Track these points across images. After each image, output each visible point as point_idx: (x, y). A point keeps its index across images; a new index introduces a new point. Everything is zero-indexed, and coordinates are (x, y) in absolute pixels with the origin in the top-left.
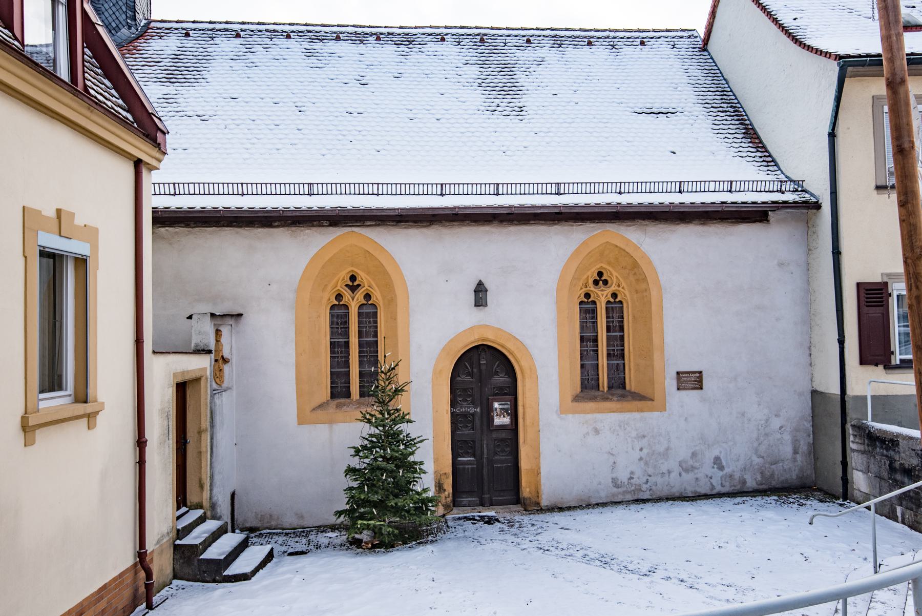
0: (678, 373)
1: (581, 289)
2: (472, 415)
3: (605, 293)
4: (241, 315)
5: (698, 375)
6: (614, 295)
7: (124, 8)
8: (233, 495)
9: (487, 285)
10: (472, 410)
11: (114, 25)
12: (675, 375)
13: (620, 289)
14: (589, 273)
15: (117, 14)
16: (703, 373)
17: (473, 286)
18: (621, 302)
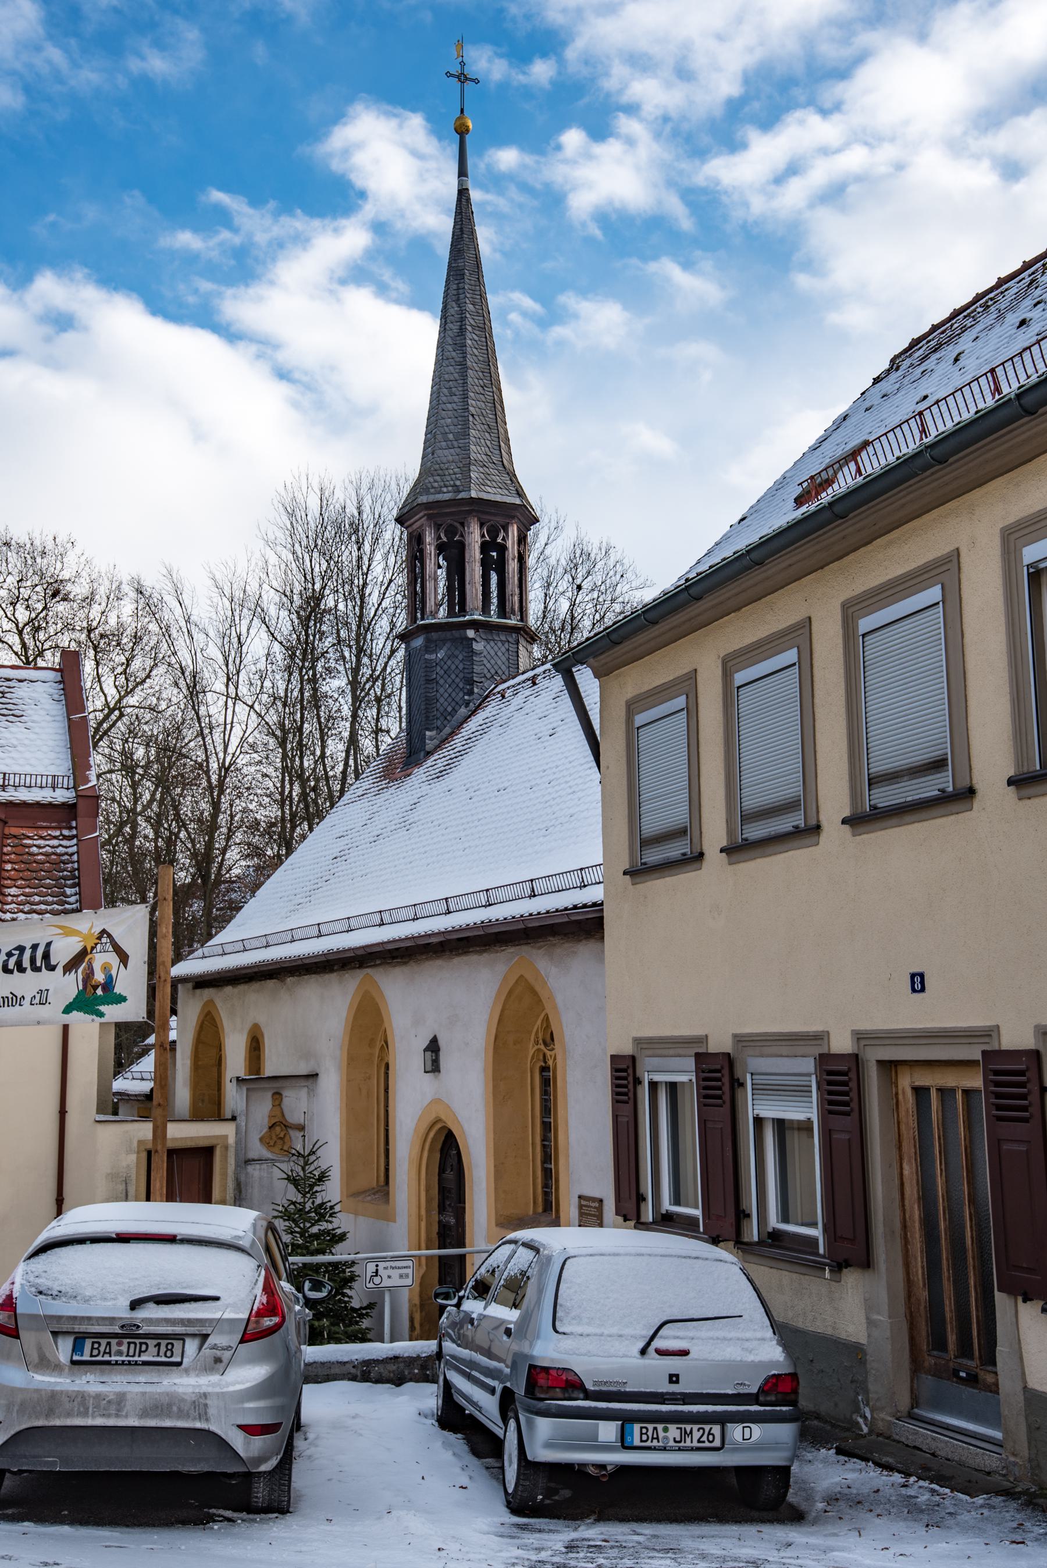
7: (461, 685)
9: (442, 1042)
11: (449, 709)
15: (454, 695)
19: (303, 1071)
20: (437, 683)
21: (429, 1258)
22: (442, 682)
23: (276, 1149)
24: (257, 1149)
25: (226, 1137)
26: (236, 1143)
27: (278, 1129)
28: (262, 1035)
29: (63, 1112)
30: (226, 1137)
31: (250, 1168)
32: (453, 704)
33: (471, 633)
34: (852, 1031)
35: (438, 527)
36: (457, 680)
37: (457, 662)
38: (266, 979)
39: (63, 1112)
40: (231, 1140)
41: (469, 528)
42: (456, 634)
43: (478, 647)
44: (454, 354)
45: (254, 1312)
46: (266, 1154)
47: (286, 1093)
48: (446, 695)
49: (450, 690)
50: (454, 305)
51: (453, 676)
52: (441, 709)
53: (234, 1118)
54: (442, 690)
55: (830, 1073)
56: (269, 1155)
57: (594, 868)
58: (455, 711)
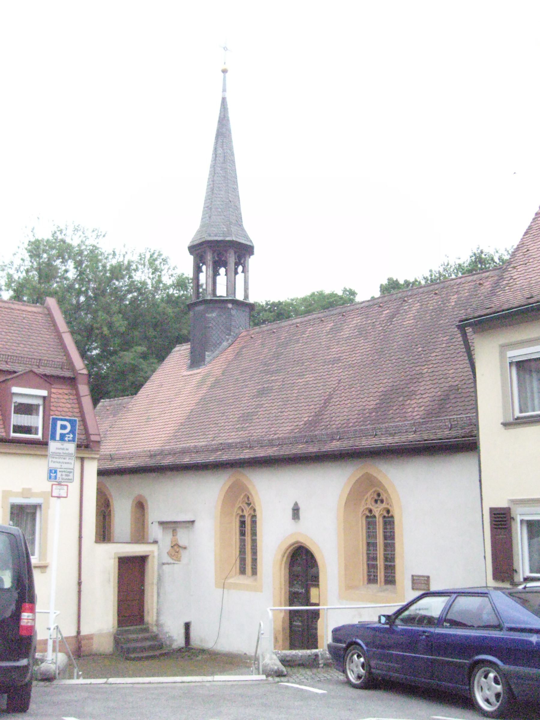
0: (413, 576)
1: (364, 506)
2: (301, 593)
3: (379, 509)
4: (296, 504)
5: (426, 579)
6: (388, 511)
8: (187, 626)
9: (301, 505)
10: (300, 591)
12: (410, 577)
13: (388, 507)
14: (369, 494)
16: (414, 574)
17: (292, 506)
18: (392, 517)
19: (188, 519)
20: (212, 328)
21: (285, 610)
22: (214, 328)
23: (174, 558)
24: (166, 559)
25: (153, 552)
26: (159, 555)
27: (176, 547)
28: (146, 501)
29: (80, 538)
30: (153, 552)
31: (165, 567)
32: (220, 339)
33: (230, 306)
34: (97, 541)
35: (214, 252)
36: (222, 328)
37: (222, 319)
38: (151, 472)
39: (80, 538)
40: (156, 554)
41: (230, 254)
42: (223, 306)
43: (233, 312)
44: (221, 172)
45: (406, 613)
46: (172, 561)
47: (178, 530)
48: (217, 335)
49: (218, 332)
50: (220, 149)
51: (221, 326)
52: (214, 342)
53: (155, 542)
54: (214, 333)
55: (495, 514)
56: (172, 561)
57: (474, 403)
58: (221, 343)
